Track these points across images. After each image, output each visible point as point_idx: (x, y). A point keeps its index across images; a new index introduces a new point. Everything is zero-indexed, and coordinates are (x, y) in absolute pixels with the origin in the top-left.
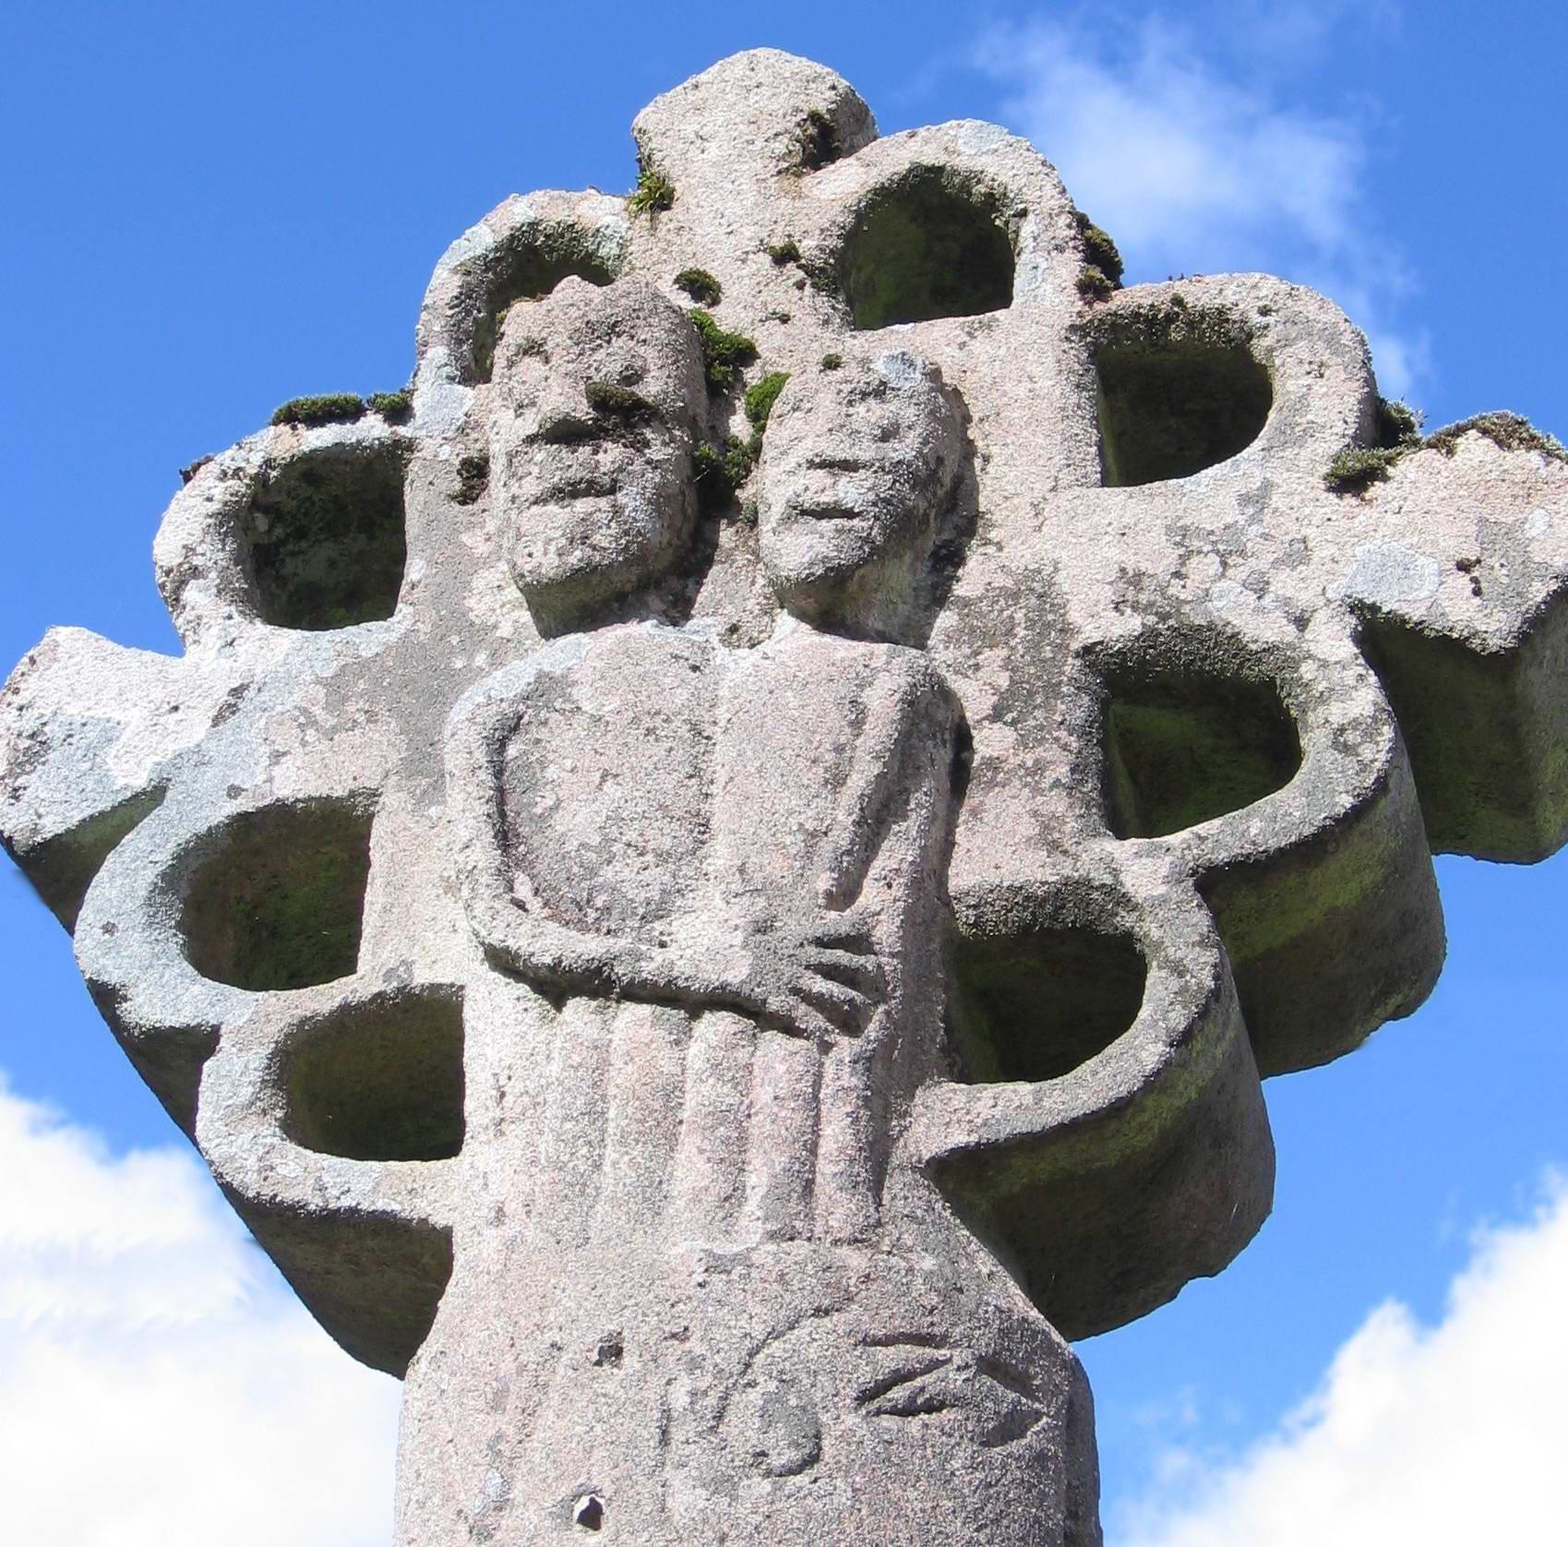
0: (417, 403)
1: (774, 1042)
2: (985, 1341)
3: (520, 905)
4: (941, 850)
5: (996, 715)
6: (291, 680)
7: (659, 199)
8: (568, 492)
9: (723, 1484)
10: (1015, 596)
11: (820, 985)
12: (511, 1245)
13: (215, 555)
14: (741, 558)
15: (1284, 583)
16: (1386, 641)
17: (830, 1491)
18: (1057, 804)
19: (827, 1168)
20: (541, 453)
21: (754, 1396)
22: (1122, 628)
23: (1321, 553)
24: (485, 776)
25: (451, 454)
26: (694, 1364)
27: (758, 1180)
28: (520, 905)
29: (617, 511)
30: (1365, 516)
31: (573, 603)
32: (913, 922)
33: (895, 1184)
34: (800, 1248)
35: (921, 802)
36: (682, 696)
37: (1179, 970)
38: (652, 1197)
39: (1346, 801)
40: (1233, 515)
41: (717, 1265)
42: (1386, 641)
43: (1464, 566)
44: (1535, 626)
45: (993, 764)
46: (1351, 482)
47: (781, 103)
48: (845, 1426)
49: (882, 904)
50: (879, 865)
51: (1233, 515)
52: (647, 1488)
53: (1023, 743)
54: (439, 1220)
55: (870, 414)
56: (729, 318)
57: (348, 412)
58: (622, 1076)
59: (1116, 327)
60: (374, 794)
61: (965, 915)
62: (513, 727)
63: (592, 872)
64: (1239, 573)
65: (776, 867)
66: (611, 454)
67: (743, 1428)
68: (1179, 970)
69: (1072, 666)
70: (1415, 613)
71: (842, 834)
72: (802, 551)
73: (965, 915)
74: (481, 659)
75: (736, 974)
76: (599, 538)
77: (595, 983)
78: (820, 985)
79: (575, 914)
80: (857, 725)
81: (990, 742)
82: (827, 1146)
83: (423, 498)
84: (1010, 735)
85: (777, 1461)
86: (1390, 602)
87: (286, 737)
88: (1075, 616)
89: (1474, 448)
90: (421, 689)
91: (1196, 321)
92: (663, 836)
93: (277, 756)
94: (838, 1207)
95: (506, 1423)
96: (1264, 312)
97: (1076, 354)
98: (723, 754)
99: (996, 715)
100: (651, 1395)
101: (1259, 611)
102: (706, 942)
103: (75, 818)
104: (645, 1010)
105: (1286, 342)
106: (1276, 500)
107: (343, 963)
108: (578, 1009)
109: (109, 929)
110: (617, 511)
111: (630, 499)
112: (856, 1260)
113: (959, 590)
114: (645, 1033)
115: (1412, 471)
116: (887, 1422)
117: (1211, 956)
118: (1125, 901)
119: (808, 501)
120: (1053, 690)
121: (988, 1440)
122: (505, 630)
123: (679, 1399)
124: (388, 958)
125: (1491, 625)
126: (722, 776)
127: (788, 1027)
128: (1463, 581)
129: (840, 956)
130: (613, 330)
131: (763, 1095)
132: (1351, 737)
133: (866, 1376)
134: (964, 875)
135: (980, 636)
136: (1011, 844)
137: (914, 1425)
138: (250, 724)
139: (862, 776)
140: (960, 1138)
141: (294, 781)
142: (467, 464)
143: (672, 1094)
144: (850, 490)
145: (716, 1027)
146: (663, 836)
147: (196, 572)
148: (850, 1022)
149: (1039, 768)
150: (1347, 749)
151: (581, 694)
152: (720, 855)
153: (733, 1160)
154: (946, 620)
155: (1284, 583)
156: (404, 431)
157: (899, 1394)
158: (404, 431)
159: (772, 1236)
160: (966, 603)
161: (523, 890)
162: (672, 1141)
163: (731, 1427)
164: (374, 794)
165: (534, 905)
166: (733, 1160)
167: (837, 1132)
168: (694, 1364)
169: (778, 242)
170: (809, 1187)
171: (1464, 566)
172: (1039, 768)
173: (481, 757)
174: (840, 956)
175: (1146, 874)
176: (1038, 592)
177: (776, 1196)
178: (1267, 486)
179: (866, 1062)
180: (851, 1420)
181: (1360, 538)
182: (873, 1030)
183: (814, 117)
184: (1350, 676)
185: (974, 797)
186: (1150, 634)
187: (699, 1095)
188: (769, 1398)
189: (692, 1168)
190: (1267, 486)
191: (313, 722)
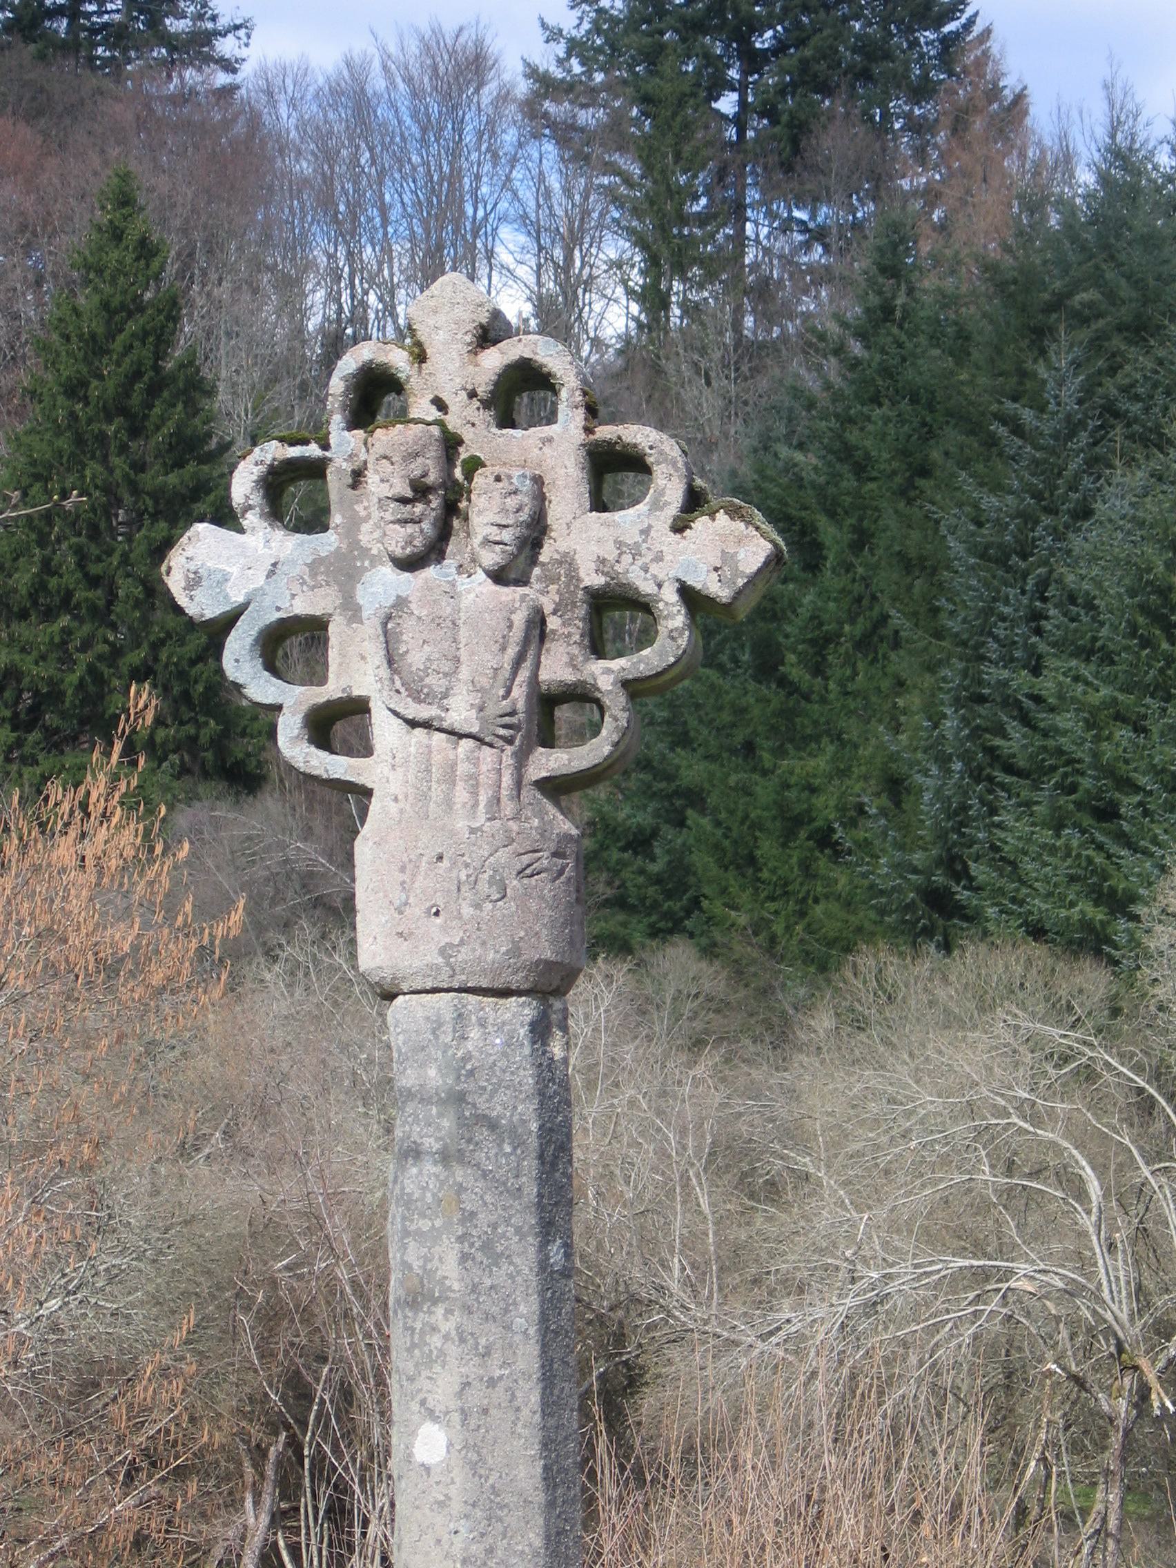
0: (332, 441)
1: (486, 750)
2: (553, 846)
3: (398, 691)
4: (537, 664)
5: (555, 613)
6: (294, 562)
7: (420, 356)
8: (404, 522)
9: (478, 906)
10: (560, 563)
11: (502, 732)
12: (401, 811)
13: (257, 499)
14: (462, 535)
15: (654, 569)
16: (688, 595)
17: (509, 906)
18: (575, 650)
19: (504, 792)
20: (393, 505)
21: (486, 876)
22: (598, 581)
23: (668, 558)
24: (382, 639)
25: (347, 467)
26: (467, 865)
27: (483, 799)
28: (398, 691)
29: (422, 531)
30: (683, 543)
31: (410, 564)
32: (529, 697)
33: (524, 792)
34: (497, 823)
35: (531, 653)
36: (449, 610)
37: (616, 719)
38: (448, 803)
39: (672, 660)
40: (638, 539)
41: (473, 831)
42: (688, 595)
43: (716, 569)
44: (739, 593)
45: (554, 632)
46: (679, 527)
47: (466, 316)
48: (513, 883)
49: (519, 693)
50: (519, 680)
51: (638, 539)
52: (453, 907)
53: (564, 624)
54: (370, 785)
55: (512, 502)
56: (453, 422)
57: (305, 442)
58: (437, 758)
59: (597, 444)
60: (330, 615)
61: (544, 687)
62: (389, 617)
63: (422, 680)
64: (639, 563)
65: (484, 682)
66: (419, 508)
67: (483, 887)
68: (616, 719)
69: (580, 594)
70: (698, 586)
71: (506, 672)
72: (491, 558)
73: (544, 687)
74: (367, 563)
75: (475, 729)
76: (416, 543)
77: (427, 725)
78: (502, 732)
79: (417, 696)
80: (510, 627)
81: (553, 623)
82: (504, 785)
83: (335, 482)
84: (559, 621)
85: (494, 898)
86: (690, 582)
87: (296, 588)
88: (582, 574)
89: (721, 516)
90: (344, 571)
91: (626, 446)
92: (446, 667)
93: (293, 596)
94: (508, 808)
95: (406, 877)
96: (651, 448)
97: (583, 452)
98: (463, 634)
99: (555, 613)
100: (454, 875)
101: (646, 579)
102: (460, 713)
103: (218, 612)
104: (443, 736)
105: (659, 463)
106: (653, 533)
107: (323, 681)
108: (418, 731)
109: (237, 661)
110: (422, 531)
111: (426, 525)
112: (513, 826)
113: (542, 558)
114: (444, 745)
115: (701, 524)
116: (526, 881)
117: (626, 715)
118: (598, 689)
119: (491, 538)
120: (574, 604)
121: (554, 880)
122: (374, 552)
123: (463, 878)
124: (343, 683)
125: (723, 593)
126: (464, 641)
127: (491, 745)
128: (715, 576)
129: (507, 720)
130: (417, 455)
131: (484, 768)
132: (675, 634)
133: (519, 867)
134: (544, 675)
135: (550, 579)
136: (557, 667)
137: (533, 880)
138: (281, 580)
139: (512, 651)
140: (544, 774)
141: (301, 607)
142: (354, 472)
143: (453, 766)
144: (507, 535)
145: (467, 744)
146: (446, 667)
147: (250, 507)
148: (510, 741)
149: (570, 635)
150: (673, 639)
151: (413, 606)
152: (464, 673)
153: (475, 794)
154: (537, 571)
155: (654, 569)
156: (327, 454)
157: (528, 871)
158: (327, 454)
159: (489, 819)
160: (543, 564)
161: (398, 684)
162: (454, 783)
163: (480, 886)
164: (330, 615)
165: (402, 690)
166: (475, 794)
167: (507, 780)
168: (467, 865)
169: (470, 387)
170: (499, 800)
171: (716, 569)
172: (570, 635)
173: (380, 631)
174: (507, 720)
175: (605, 674)
176: (567, 561)
177: (489, 805)
178: (650, 527)
179: (515, 754)
180: (515, 882)
181: (682, 553)
182: (517, 742)
183: (481, 326)
184: (675, 609)
185: (547, 645)
186: (607, 584)
187: (463, 768)
188: (492, 877)
189: (461, 795)
190: (650, 527)
191: (304, 583)
